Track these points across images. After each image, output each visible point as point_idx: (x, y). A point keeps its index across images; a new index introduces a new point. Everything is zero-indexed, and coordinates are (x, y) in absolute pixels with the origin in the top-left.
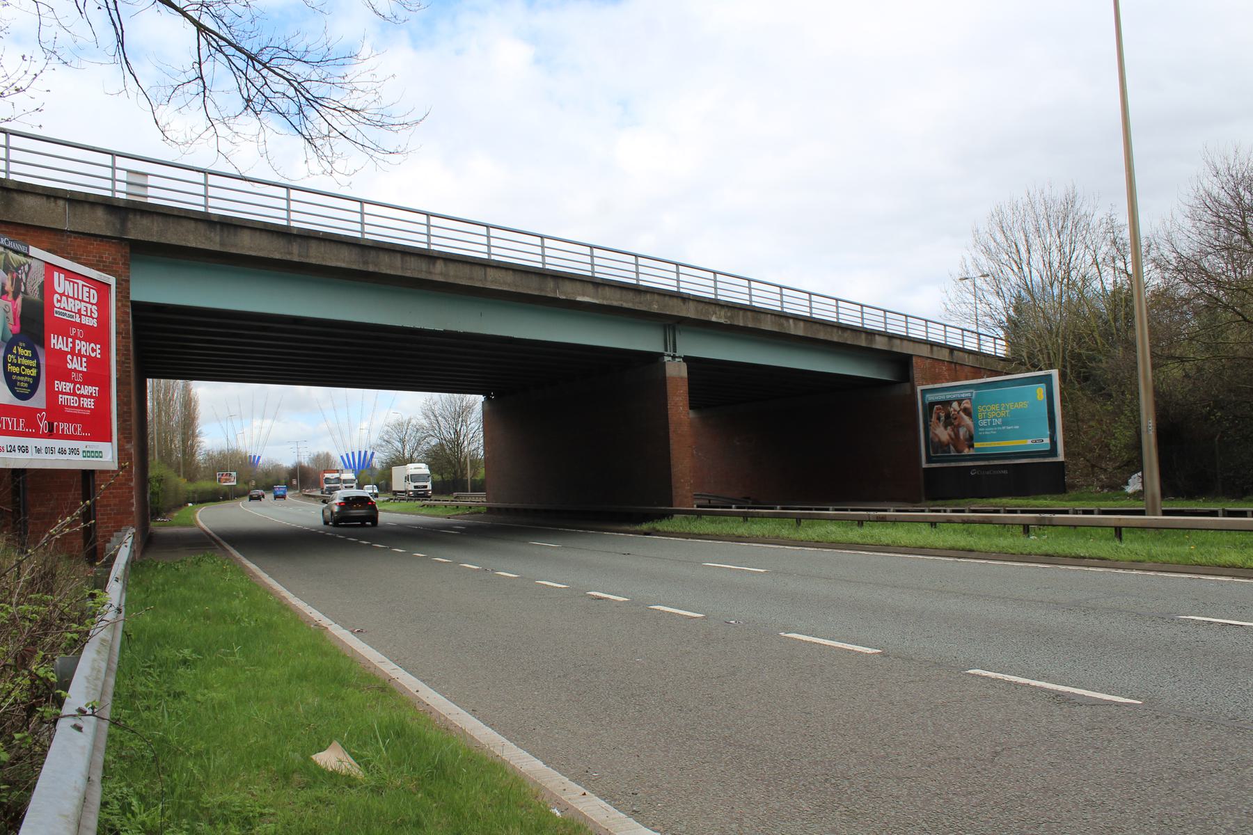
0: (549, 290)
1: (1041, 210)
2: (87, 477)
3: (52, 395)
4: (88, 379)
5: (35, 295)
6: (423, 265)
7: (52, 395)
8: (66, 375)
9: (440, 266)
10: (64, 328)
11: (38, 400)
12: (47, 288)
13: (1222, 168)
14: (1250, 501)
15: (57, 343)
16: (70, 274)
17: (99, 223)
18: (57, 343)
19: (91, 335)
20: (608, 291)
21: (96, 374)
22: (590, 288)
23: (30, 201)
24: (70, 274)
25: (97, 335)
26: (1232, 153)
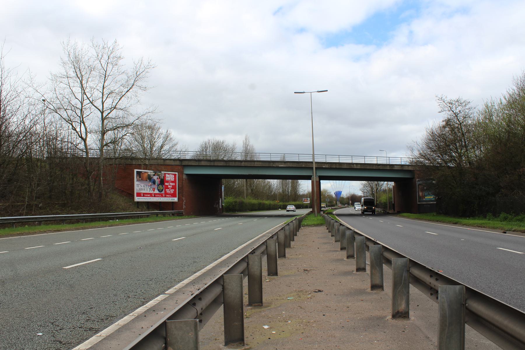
0: (271, 165)
1: (519, 79)
2: (173, 203)
3: (165, 191)
4: (172, 188)
5: (162, 178)
6: (239, 163)
7: (165, 191)
8: (168, 188)
9: (243, 163)
10: (168, 182)
11: (163, 192)
12: (165, 177)
13: (515, 78)
14: (521, 220)
15: (166, 184)
16: (168, 174)
17: (178, 163)
18: (166, 184)
19: (172, 182)
20: (288, 164)
21: (174, 187)
22: (283, 163)
23: (168, 161)
24: (168, 174)
25: (174, 182)
26: (72, 51)
